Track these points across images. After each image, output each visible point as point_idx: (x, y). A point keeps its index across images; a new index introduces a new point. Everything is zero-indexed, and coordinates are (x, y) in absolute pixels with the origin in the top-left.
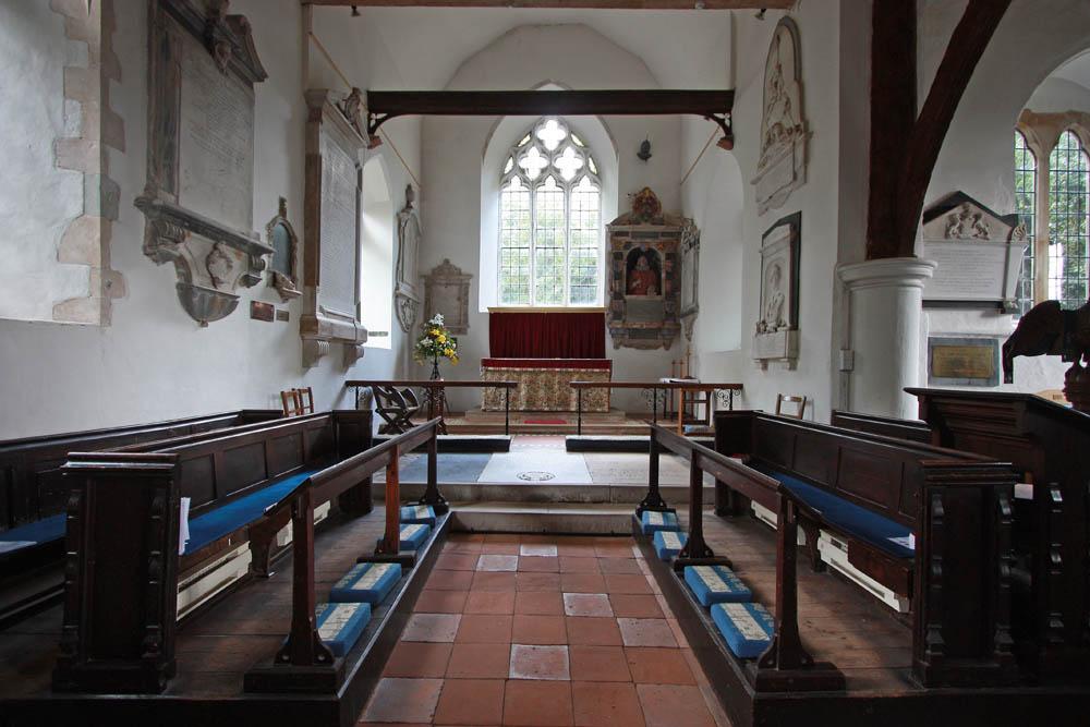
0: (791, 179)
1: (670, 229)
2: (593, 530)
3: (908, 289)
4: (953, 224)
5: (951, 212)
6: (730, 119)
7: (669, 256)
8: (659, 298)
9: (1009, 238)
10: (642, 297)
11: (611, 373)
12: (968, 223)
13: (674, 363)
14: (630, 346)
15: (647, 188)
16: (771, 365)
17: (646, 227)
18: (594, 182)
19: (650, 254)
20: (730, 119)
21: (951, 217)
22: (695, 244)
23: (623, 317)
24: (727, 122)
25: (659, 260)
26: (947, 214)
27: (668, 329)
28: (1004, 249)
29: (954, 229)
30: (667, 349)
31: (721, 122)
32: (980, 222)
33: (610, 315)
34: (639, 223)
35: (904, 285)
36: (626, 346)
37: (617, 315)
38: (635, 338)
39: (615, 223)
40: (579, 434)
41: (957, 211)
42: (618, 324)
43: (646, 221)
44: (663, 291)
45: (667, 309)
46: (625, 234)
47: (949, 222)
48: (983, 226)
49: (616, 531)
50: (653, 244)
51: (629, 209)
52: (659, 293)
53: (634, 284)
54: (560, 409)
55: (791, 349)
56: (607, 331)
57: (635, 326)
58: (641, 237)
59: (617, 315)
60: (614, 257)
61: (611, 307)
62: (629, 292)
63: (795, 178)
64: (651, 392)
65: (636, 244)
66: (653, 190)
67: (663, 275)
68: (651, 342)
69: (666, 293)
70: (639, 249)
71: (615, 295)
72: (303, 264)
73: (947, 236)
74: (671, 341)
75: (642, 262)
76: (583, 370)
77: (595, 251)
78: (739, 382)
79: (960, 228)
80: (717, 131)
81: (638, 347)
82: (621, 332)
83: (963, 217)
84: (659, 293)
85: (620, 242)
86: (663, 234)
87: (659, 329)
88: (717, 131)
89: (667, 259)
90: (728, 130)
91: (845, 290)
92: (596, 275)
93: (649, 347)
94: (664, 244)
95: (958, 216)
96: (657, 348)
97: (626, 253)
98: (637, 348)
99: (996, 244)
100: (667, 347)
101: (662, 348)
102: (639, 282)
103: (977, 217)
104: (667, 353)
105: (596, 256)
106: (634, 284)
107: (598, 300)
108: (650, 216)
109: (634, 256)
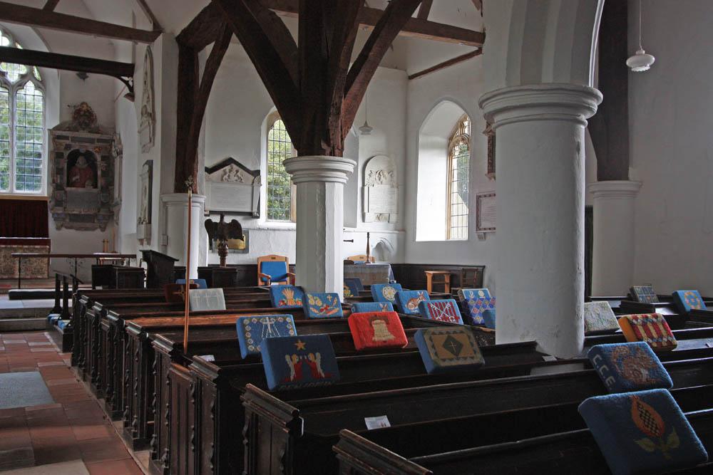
0: (149, 141)
1: (105, 137)
2: (23, 328)
3: (329, 174)
4: (225, 174)
5: (224, 168)
6: (133, 81)
7: (103, 158)
8: (95, 191)
9: (253, 182)
10: (81, 190)
11: (50, 249)
12: (232, 174)
13: (104, 242)
14: (71, 228)
15: (83, 103)
16: (402, 232)
17: (84, 134)
18: (37, 87)
19: (89, 156)
20: (133, 81)
21: (224, 171)
22: (120, 153)
23: (64, 205)
24: (131, 83)
25: (96, 160)
26: (222, 169)
27: (103, 215)
28: (251, 188)
29: (226, 177)
30: (102, 231)
31: (126, 83)
32: (238, 174)
33: (53, 203)
34: (78, 131)
35: (450, 154)
36: (67, 228)
37: (59, 203)
38: (78, 221)
39: (56, 128)
40: (19, 288)
41: (227, 168)
42: (60, 210)
43: (84, 129)
44: (99, 185)
45: (103, 200)
46: (67, 138)
47: (223, 173)
48: (240, 176)
49: (36, 328)
50: (90, 148)
51: (68, 118)
52: (95, 186)
53: (74, 179)
54: (5, 277)
55: (147, 235)
56: (50, 215)
57: (74, 212)
58: (79, 142)
59: (59, 203)
60: (56, 156)
61: (53, 196)
62: (70, 184)
63: (150, 141)
64: (73, 260)
65: (76, 146)
66: (89, 105)
67: (99, 173)
68: (88, 225)
69: (102, 188)
70: (78, 150)
71: (56, 186)
72: (268, 356)
73: (222, 180)
74: (106, 225)
75: (81, 161)
76: (26, 247)
77: (39, 146)
78: (133, 254)
79: (229, 176)
80: (124, 88)
81: (78, 229)
82: (63, 216)
83: (230, 171)
84: (95, 186)
85: (61, 144)
86: (99, 140)
87: (95, 216)
88: (124, 88)
89: (102, 160)
90: (131, 89)
91: (164, 206)
92: (41, 166)
93: (87, 229)
94: (99, 148)
95: (227, 171)
96: (94, 229)
97: (66, 153)
98: (77, 229)
99: (247, 185)
100: (103, 229)
101: (99, 230)
102: (78, 177)
103: (237, 171)
104: (101, 233)
105: (41, 151)
106: (74, 179)
107: (42, 190)
108: (87, 125)
109: (74, 156)
